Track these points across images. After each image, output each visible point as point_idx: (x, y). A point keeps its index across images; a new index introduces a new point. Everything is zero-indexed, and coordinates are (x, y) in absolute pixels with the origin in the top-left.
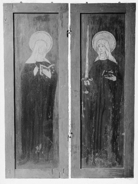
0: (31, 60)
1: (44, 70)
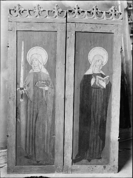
0: (89, 72)
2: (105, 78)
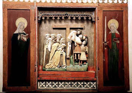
0: (15, 33)
1: (23, 37)
2: (26, 35)
